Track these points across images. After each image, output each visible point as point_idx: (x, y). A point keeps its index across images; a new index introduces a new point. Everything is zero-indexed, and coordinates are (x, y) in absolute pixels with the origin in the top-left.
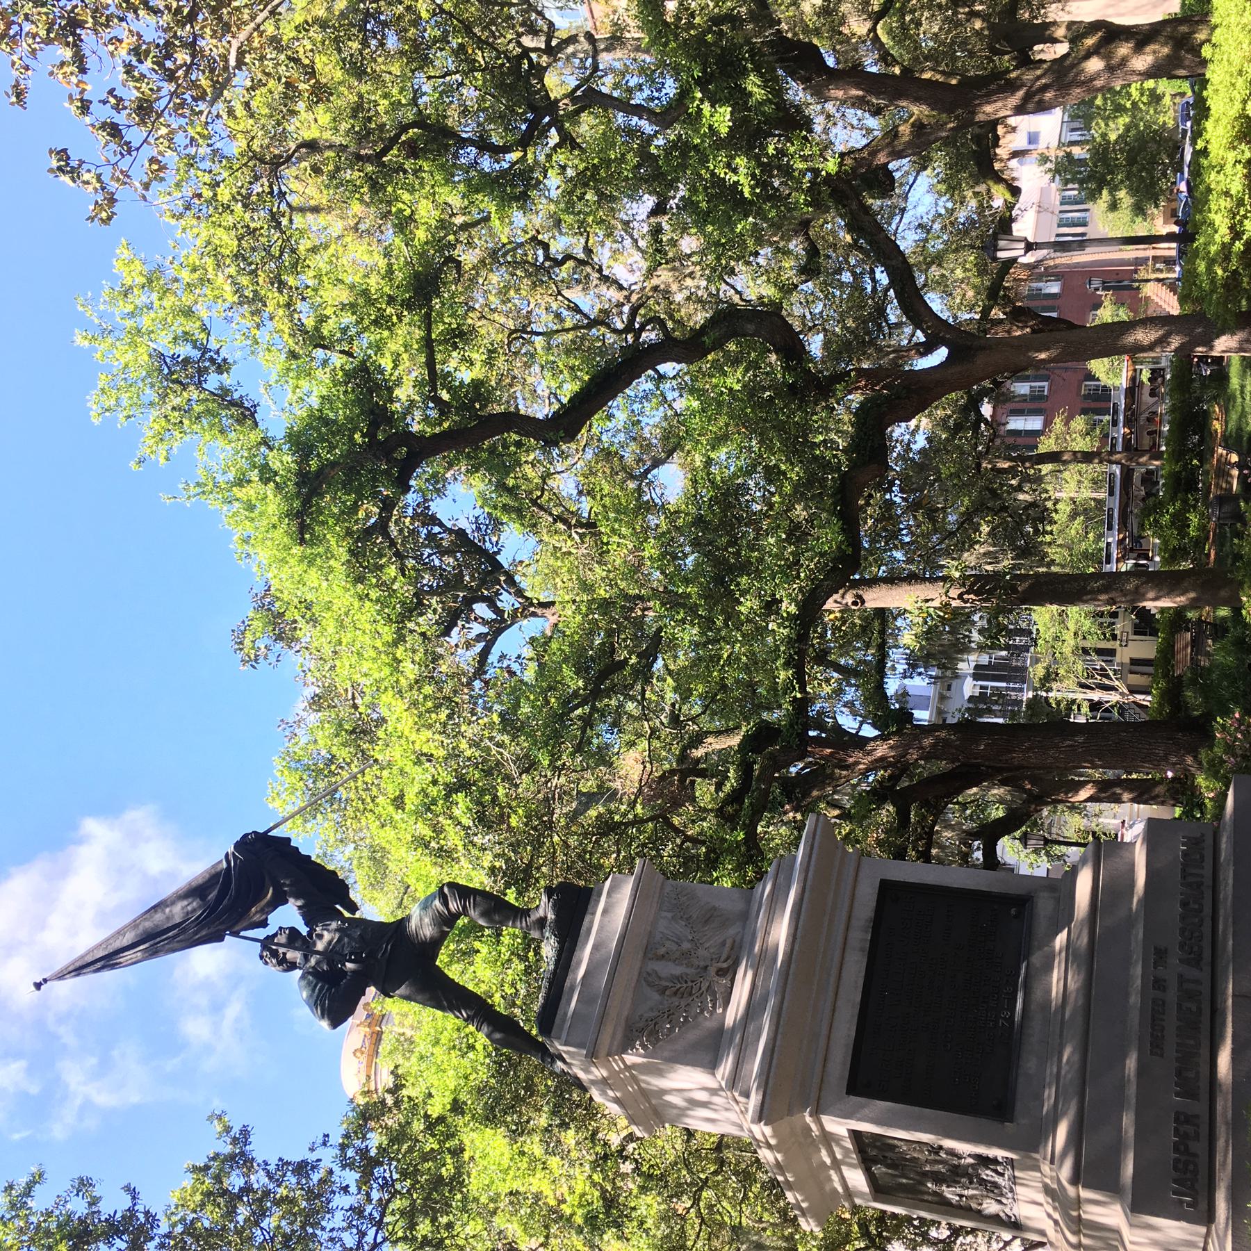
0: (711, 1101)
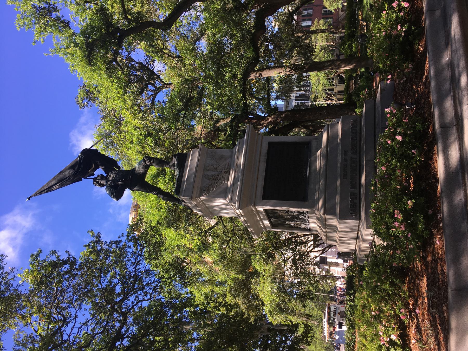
0: (226, 206)
